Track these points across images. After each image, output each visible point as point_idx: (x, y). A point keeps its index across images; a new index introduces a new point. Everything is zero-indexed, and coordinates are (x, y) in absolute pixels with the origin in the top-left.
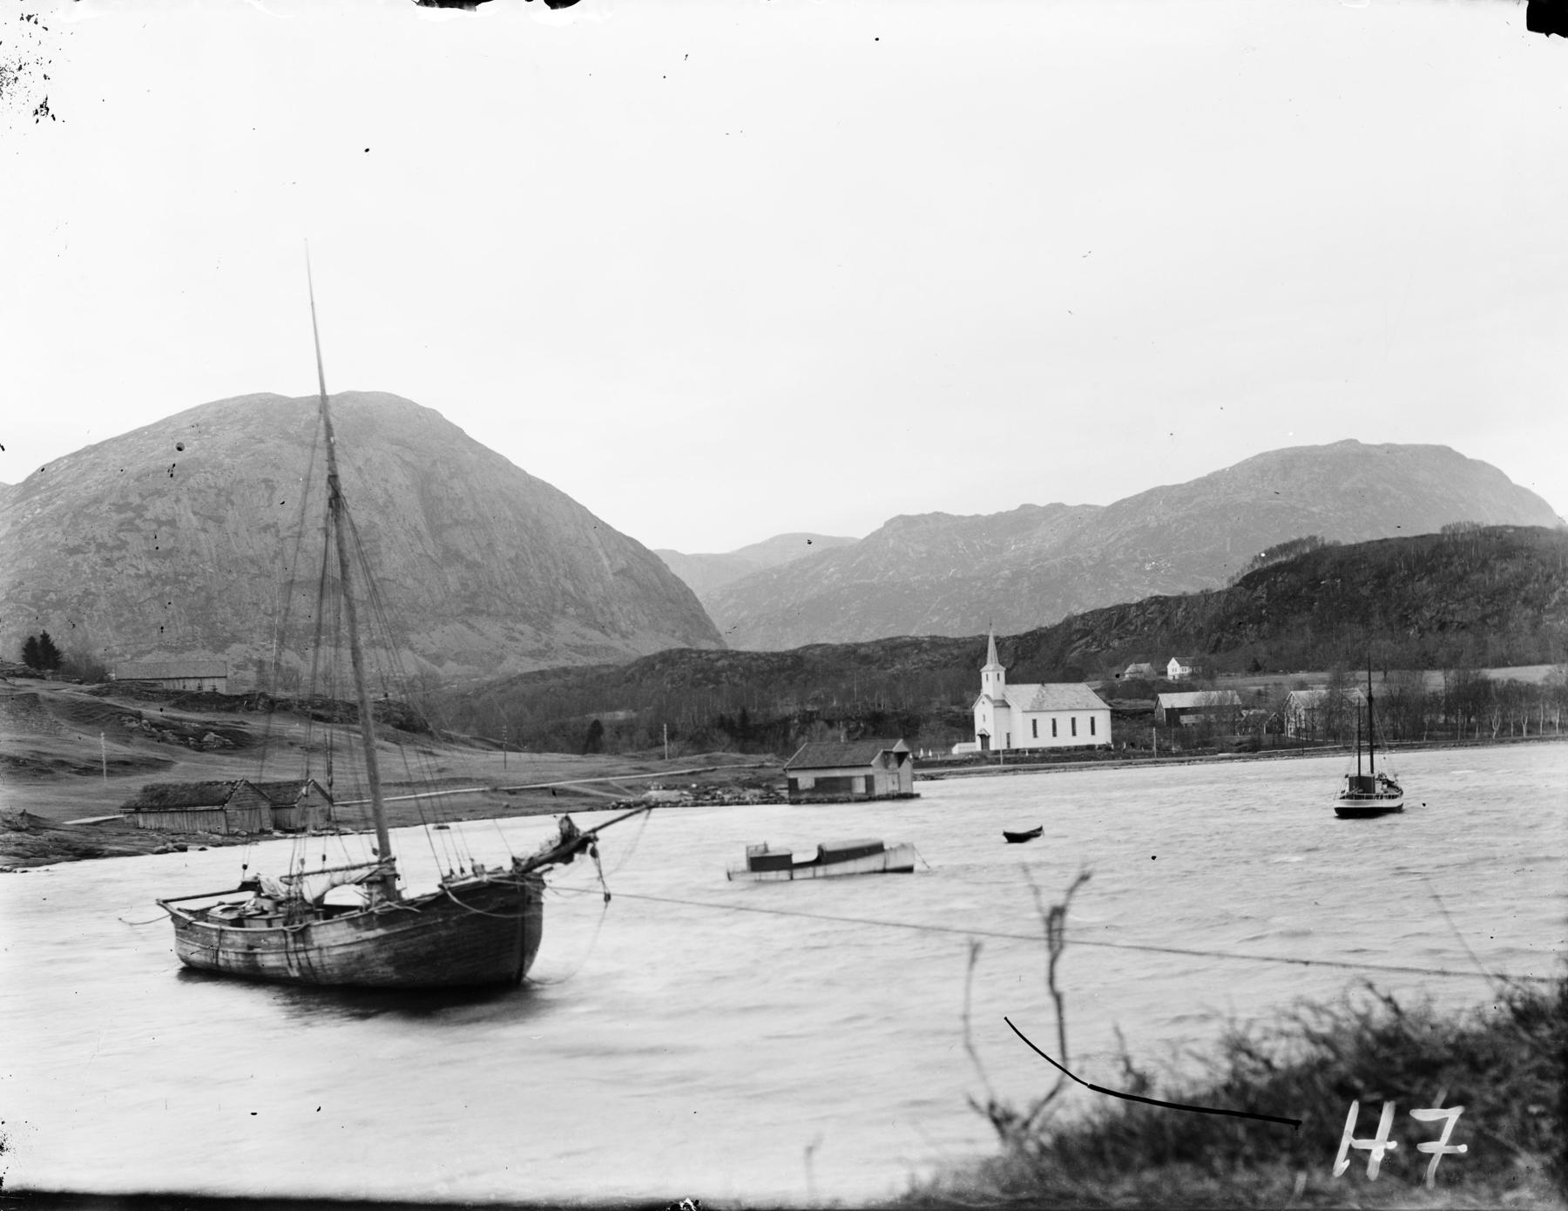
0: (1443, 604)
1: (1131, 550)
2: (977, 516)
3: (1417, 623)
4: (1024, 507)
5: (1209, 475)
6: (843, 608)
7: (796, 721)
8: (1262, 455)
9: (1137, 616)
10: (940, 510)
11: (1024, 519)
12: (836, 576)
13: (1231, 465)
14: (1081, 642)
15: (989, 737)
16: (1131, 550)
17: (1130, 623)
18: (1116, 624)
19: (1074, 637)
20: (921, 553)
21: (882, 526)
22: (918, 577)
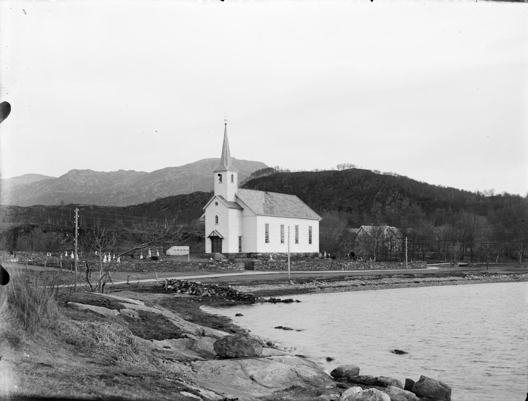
0: (341, 199)
1: (159, 188)
2: (103, 172)
3: (328, 207)
4: (120, 170)
5: (186, 165)
6: (51, 201)
7: (22, 231)
8: (204, 160)
9: (190, 200)
10: (89, 169)
11: (120, 175)
12: (49, 189)
13: (194, 162)
14: (164, 210)
15: (221, 239)
16: (159, 188)
17: (187, 202)
18: (180, 203)
19: (161, 208)
20: (82, 183)
21: (67, 172)
22: (81, 192)
